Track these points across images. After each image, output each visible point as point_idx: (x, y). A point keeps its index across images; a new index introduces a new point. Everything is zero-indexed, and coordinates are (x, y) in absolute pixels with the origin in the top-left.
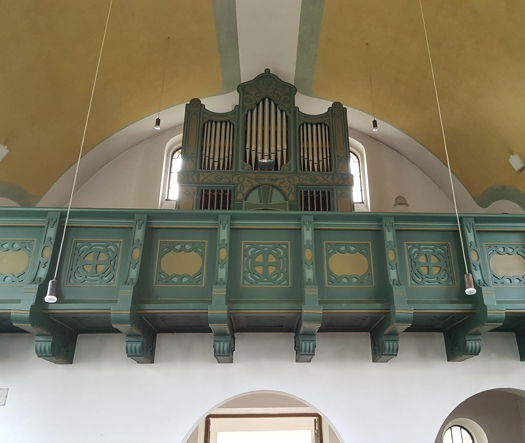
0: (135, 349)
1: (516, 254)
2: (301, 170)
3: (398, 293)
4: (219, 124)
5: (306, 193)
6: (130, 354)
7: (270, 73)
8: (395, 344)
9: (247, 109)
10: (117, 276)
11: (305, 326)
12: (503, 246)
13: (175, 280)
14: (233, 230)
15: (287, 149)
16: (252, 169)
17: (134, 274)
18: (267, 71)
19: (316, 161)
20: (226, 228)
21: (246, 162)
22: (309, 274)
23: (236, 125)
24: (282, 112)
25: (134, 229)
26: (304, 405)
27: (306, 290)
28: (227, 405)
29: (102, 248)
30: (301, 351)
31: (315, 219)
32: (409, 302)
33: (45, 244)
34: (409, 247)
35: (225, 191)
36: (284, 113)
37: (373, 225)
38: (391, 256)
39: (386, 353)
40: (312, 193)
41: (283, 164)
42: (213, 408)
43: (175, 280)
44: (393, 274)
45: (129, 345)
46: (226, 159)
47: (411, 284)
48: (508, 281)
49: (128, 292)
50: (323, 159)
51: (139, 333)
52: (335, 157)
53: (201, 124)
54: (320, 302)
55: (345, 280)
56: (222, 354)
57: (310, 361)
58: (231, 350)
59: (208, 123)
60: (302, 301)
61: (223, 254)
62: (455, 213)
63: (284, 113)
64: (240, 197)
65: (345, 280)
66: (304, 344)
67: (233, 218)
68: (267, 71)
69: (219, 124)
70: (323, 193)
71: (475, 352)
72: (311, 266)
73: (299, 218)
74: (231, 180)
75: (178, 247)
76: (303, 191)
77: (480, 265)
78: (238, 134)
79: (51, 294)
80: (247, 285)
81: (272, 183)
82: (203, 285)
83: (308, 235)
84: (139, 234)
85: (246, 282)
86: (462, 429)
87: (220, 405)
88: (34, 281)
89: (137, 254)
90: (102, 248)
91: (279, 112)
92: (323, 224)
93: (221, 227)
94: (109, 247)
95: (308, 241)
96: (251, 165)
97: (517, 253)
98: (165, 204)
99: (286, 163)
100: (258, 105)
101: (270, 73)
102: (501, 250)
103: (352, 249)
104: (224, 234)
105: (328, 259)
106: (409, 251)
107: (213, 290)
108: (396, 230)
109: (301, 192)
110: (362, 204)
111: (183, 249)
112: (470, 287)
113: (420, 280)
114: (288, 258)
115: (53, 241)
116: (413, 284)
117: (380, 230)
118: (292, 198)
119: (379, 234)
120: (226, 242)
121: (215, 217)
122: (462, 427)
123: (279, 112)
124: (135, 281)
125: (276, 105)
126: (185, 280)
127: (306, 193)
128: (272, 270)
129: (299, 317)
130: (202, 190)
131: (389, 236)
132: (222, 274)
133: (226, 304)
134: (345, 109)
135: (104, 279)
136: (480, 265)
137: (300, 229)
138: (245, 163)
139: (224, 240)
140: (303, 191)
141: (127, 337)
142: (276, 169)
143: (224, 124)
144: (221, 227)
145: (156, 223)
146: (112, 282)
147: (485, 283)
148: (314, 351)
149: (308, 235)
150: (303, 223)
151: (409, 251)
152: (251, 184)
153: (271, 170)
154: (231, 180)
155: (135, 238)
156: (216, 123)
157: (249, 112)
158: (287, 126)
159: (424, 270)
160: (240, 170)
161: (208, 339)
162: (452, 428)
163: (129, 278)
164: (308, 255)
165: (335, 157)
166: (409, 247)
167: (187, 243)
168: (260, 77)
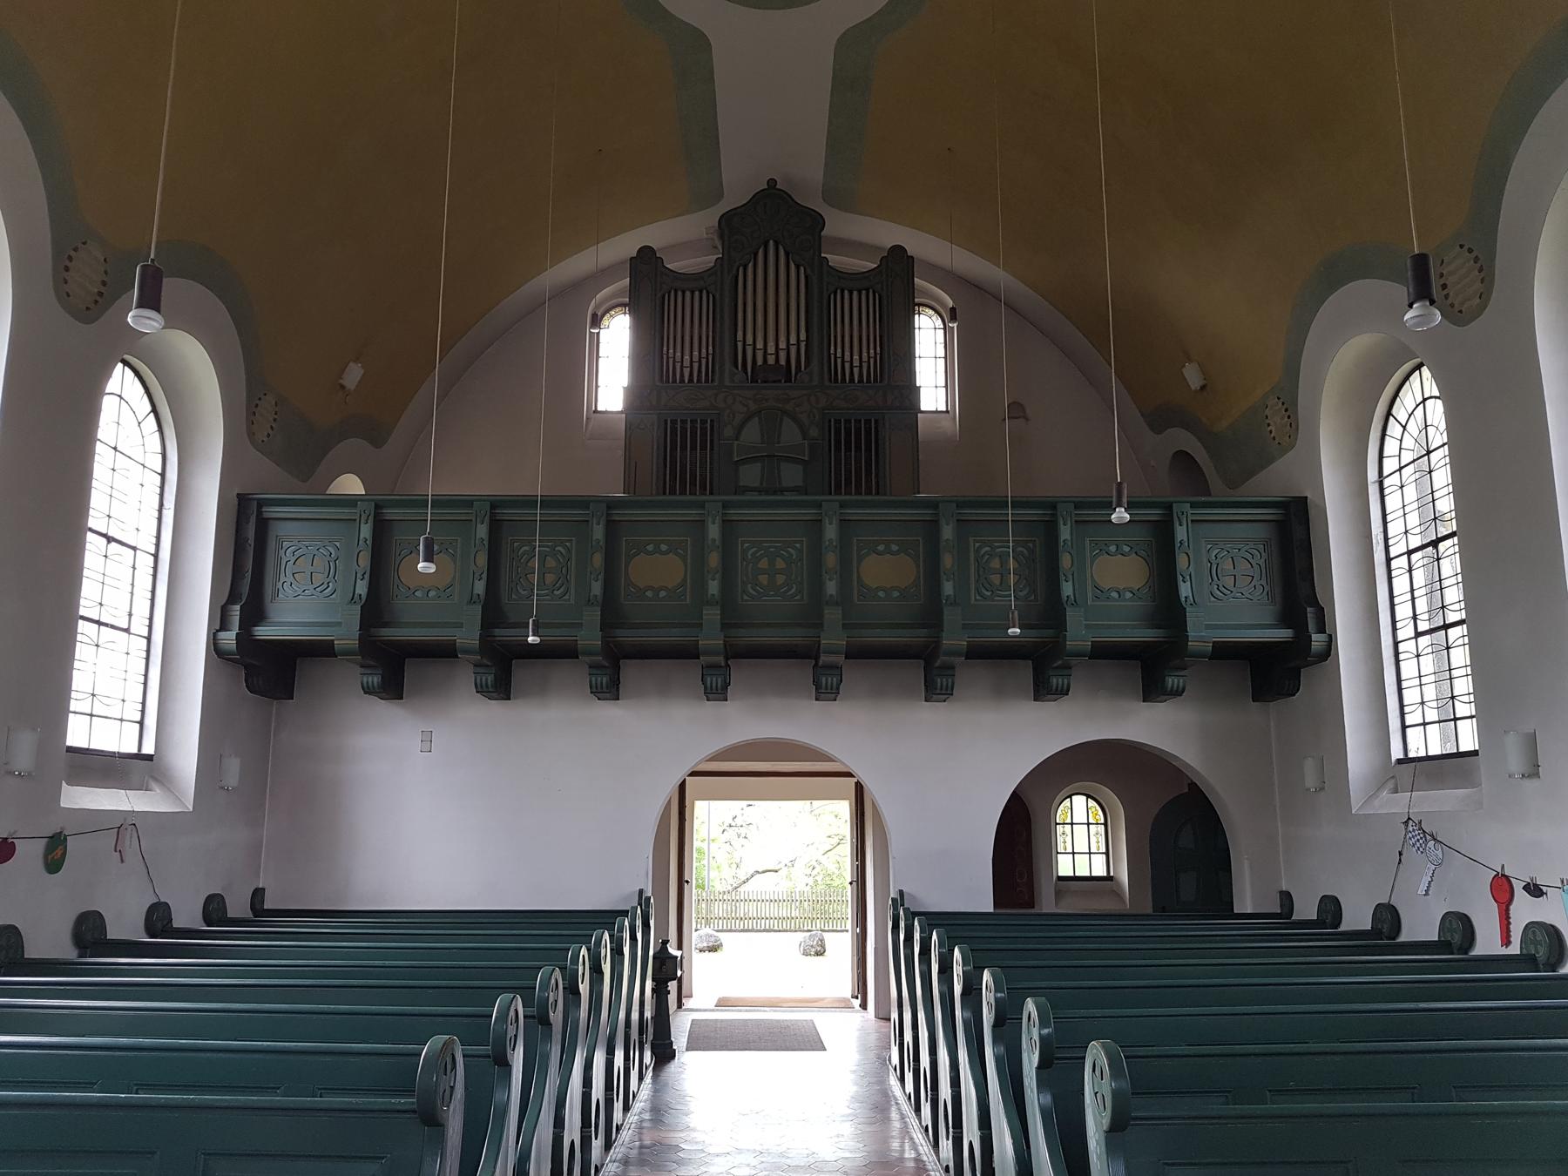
0: (602, 683)
1: (1134, 555)
2: (831, 381)
3: (951, 616)
4: (688, 294)
5: (838, 422)
6: (594, 690)
7: (778, 187)
8: (950, 680)
9: (737, 264)
10: (573, 591)
11: (824, 659)
12: (1116, 543)
13: (649, 594)
14: (727, 523)
15: (807, 340)
16: (748, 379)
17: (597, 588)
18: (772, 183)
19: (856, 363)
20: (717, 521)
21: (737, 368)
22: (831, 588)
23: (717, 296)
24: (798, 267)
25: (590, 523)
26: (829, 759)
27: (826, 611)
28: (713, 758)
29: (548, 549)
30: (821, 688)
31: (843, 505)
32: (965, 626)
33: (476, 549)
34: (977, 545)
35: (703, 422)
36: (802, 268)
37: (926, 513)
38: (947, 561)
39: (938, 692)
40: (848, 421)
41: (800, 371)
42: (697, 764)
43: (649, 594)
44: (948, 588)
45: (593, 679)
46: (704, 361)
47: (976, 600)
48: (1115, 595)
49: (594, 616)
50: (869, 358)
51: (607, 665)
52: (889, 354)
53: (659, 295)
54: (845, 626)
55: (881, 594)
56: (714, 691)
57: (835, 700)
58: (726, 685)
59: (669, 293)
60: (820, 626)
61: (714, 560)
62: (466, 1059)
63: (802, 268)
64: (728, 432)
65: (881, 594)
66: (824, 679)
67: (726, 505)
68: (772, 183)
69: (688, 294)
70: (868, 422)
71: (1062, 690)
72: (835, 576)
73: (819, 505)
74: (713, 402)
75: (650, 548)
76: (832, 420)
77: (1073, 575)
78: (722, 317)
79: (533, 635)
80: (746, 601)
81: (780, 405)
82: (688, 601)
83: (831, 532)
84: (598, 532)
85: (746, 597)
86: (1089, 800)
87: (708, 758)
88: (471, 602)
89: (598, 560)
90: (548, 549)
91: (793, 266)
92: (853, 513)
93: (710, 519)
94: (557, 549)
95: (831, 541)
96: (746, 373)
97: (1136, 553)
98: (592, 420)
99: (805, 369)
100: (756, 254)
101: (778, 187)
102: (1113, 548)
103: (895, 548)
104: (714, 531)
105: (859, 563)
106: (977, 551)
107: (704, 612)
108: (958, 520)
109: (830, 421)
110: (947, 415)
111: (658, 551)
112: (1014, 627)
113: (989, 593)
114: (802, 564)
115: (486, 542)
116: (978, 600)
117: (936, 521)
118: (814, 432)
119: (932, 527)
120: (717, 542)
121: (702, 505)
122: (1088, 796)
123: (793, 266)
124: (600, 598)
125: (787, 254)
126: (663, 594)
127: (838, 422)
128: (780, 579)
129: (817, 645)
130: (666, 421)
131: (947, 532)
132: (714, 587)
133: (721, 631)
134: (911, 260)
135: (555, 592)
136: (1073, 575)
137: (821, 520)
138: (736, 371)
139: (714, 540)
140: (832, 420)
141: (236, 501)
142: (788, 380)
143: (697, 293)
144: (710, 519)
145: (618, 514)
146: (566, 597)
147: (1075, 601)
148: (838, 688)
149: (831, 532)
150: (823, 514)
151: (977, 551)
152: (745, 409)
153: (780, 381)
154: (713, 402)
155: (594, 538)
156: (684, 292)
157: (741, 269)
158: (807, 293)
159: (996, 579)
160: (727, 383)
161: (692, 670)
162: (1073, 797)
163: (592, 594)
164: (831, 560)
165: (889, 354)
166: (977, 545)
167: (662, 542)
168: (758, 198)
